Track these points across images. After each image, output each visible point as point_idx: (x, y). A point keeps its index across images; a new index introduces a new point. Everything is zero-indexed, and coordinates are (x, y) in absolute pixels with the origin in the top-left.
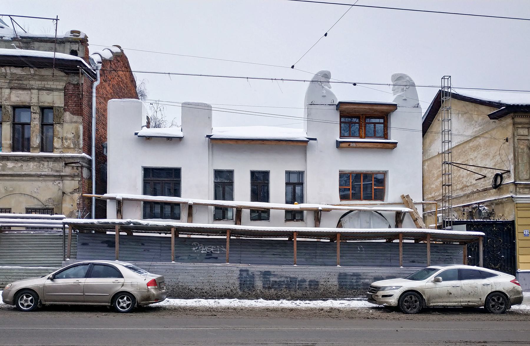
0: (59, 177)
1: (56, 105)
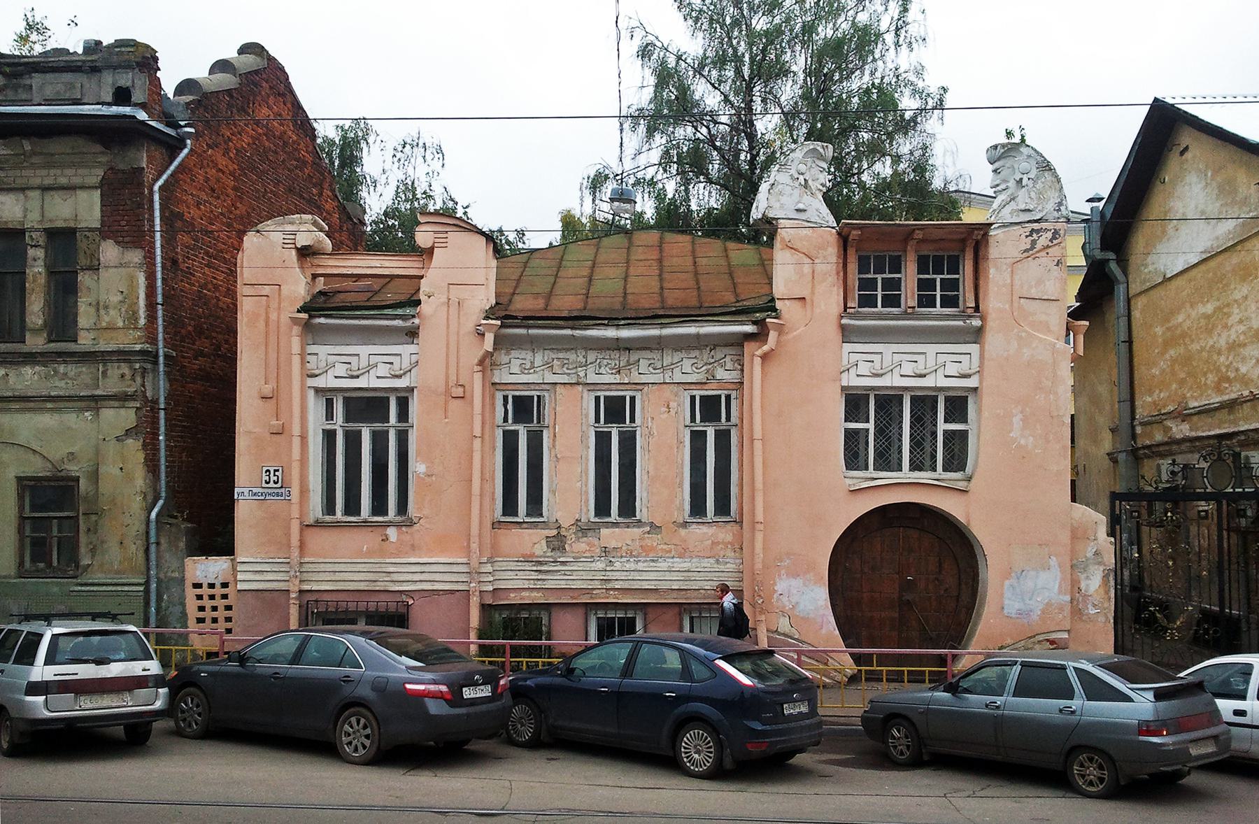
0: (90, 401)
1: (83, 225)
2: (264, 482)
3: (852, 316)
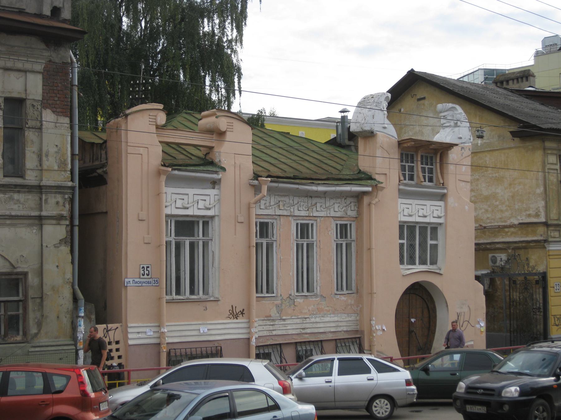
2: (141, 274)
3: (406, 185)
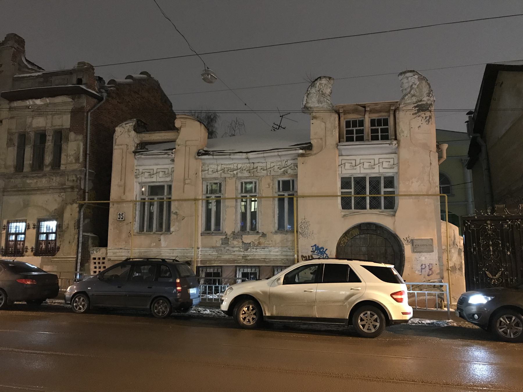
1: (64, 127)
